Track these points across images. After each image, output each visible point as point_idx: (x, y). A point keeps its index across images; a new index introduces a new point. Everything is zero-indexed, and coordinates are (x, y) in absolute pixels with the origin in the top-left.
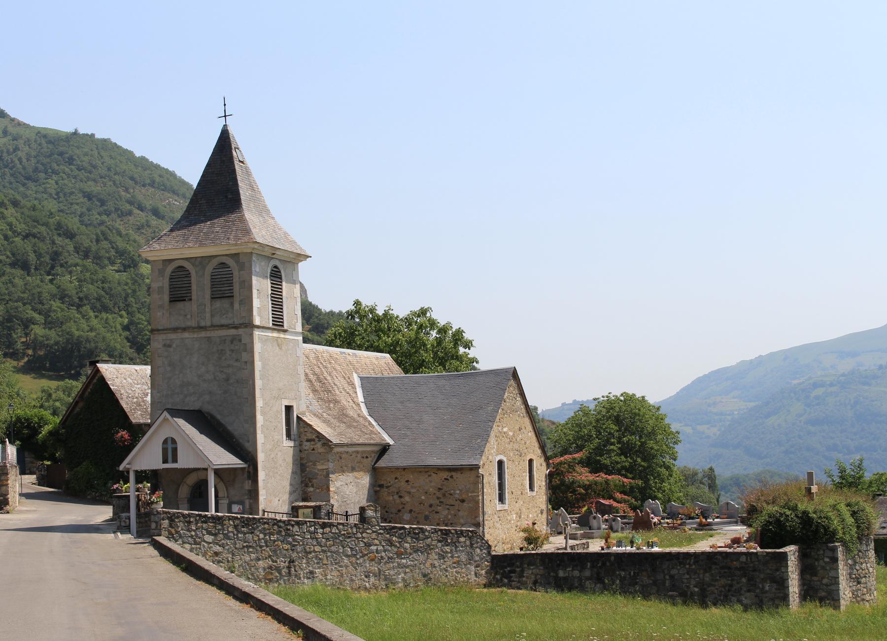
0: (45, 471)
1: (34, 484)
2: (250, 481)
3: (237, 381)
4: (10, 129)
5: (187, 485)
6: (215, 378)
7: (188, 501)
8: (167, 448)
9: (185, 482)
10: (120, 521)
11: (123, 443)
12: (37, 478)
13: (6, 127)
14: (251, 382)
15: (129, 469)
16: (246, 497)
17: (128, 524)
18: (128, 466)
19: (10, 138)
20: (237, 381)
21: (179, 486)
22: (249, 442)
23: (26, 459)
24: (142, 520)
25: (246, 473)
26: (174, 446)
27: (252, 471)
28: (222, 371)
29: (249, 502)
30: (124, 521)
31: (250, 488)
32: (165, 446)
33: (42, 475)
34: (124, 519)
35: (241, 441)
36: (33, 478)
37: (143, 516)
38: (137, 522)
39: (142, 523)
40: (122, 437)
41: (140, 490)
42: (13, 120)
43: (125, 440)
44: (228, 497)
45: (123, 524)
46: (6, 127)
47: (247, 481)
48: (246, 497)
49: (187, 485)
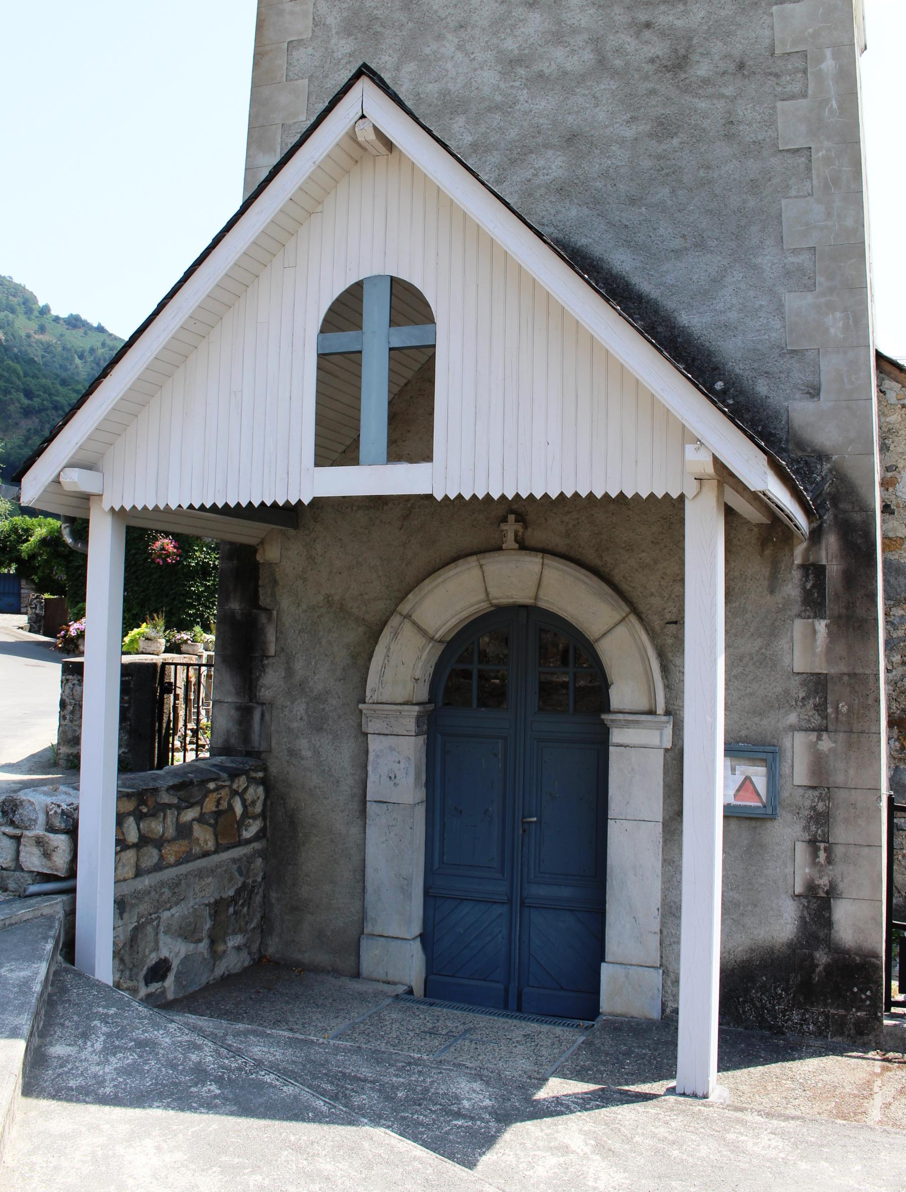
0: (41, 609)
1: (22, 628)
2: (821, 626)
3: (741, 66)
4: (108, 342)
5: (423, 632)
6: (602, 62)
7: (419, 720)
8: (354, 357)
9: (408, 616)
10: (17, 839)
11: (165, 560)
12: (29, 619)
13: (105, 340)
14: (829, 65)
15: (86, 498)
16: (792, 718)
17: (60, 861)
18: (76, 480)
19: (107, 349)
20: (741, 66)
21: (374, 635)
22: (814, 392)
23: (22, 591)
24: (156, 827)
25: (797, 575)
26: (406, 336)
27: (834, 568)
28: (648, 25)
29: (813, 747)
30: (39, 842)
31: (821, 667)
32: (342, 341)
33: (37, 615)
34: (39, 830)
35: (762, 388)
36: (22, 620)
37: (166, 798)
38: (121, 844)
39: (159, 843)
40: (163, 549)
41: (184, 648)
42: (111, 335)
43: (168, 555)
44: (668, 713)
45: (32, 860)
46: (105, 340)
47: (799, 625)
48: (792, 718)
49: (423, 632)
